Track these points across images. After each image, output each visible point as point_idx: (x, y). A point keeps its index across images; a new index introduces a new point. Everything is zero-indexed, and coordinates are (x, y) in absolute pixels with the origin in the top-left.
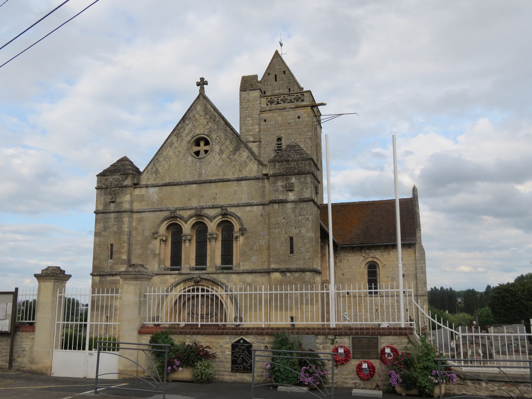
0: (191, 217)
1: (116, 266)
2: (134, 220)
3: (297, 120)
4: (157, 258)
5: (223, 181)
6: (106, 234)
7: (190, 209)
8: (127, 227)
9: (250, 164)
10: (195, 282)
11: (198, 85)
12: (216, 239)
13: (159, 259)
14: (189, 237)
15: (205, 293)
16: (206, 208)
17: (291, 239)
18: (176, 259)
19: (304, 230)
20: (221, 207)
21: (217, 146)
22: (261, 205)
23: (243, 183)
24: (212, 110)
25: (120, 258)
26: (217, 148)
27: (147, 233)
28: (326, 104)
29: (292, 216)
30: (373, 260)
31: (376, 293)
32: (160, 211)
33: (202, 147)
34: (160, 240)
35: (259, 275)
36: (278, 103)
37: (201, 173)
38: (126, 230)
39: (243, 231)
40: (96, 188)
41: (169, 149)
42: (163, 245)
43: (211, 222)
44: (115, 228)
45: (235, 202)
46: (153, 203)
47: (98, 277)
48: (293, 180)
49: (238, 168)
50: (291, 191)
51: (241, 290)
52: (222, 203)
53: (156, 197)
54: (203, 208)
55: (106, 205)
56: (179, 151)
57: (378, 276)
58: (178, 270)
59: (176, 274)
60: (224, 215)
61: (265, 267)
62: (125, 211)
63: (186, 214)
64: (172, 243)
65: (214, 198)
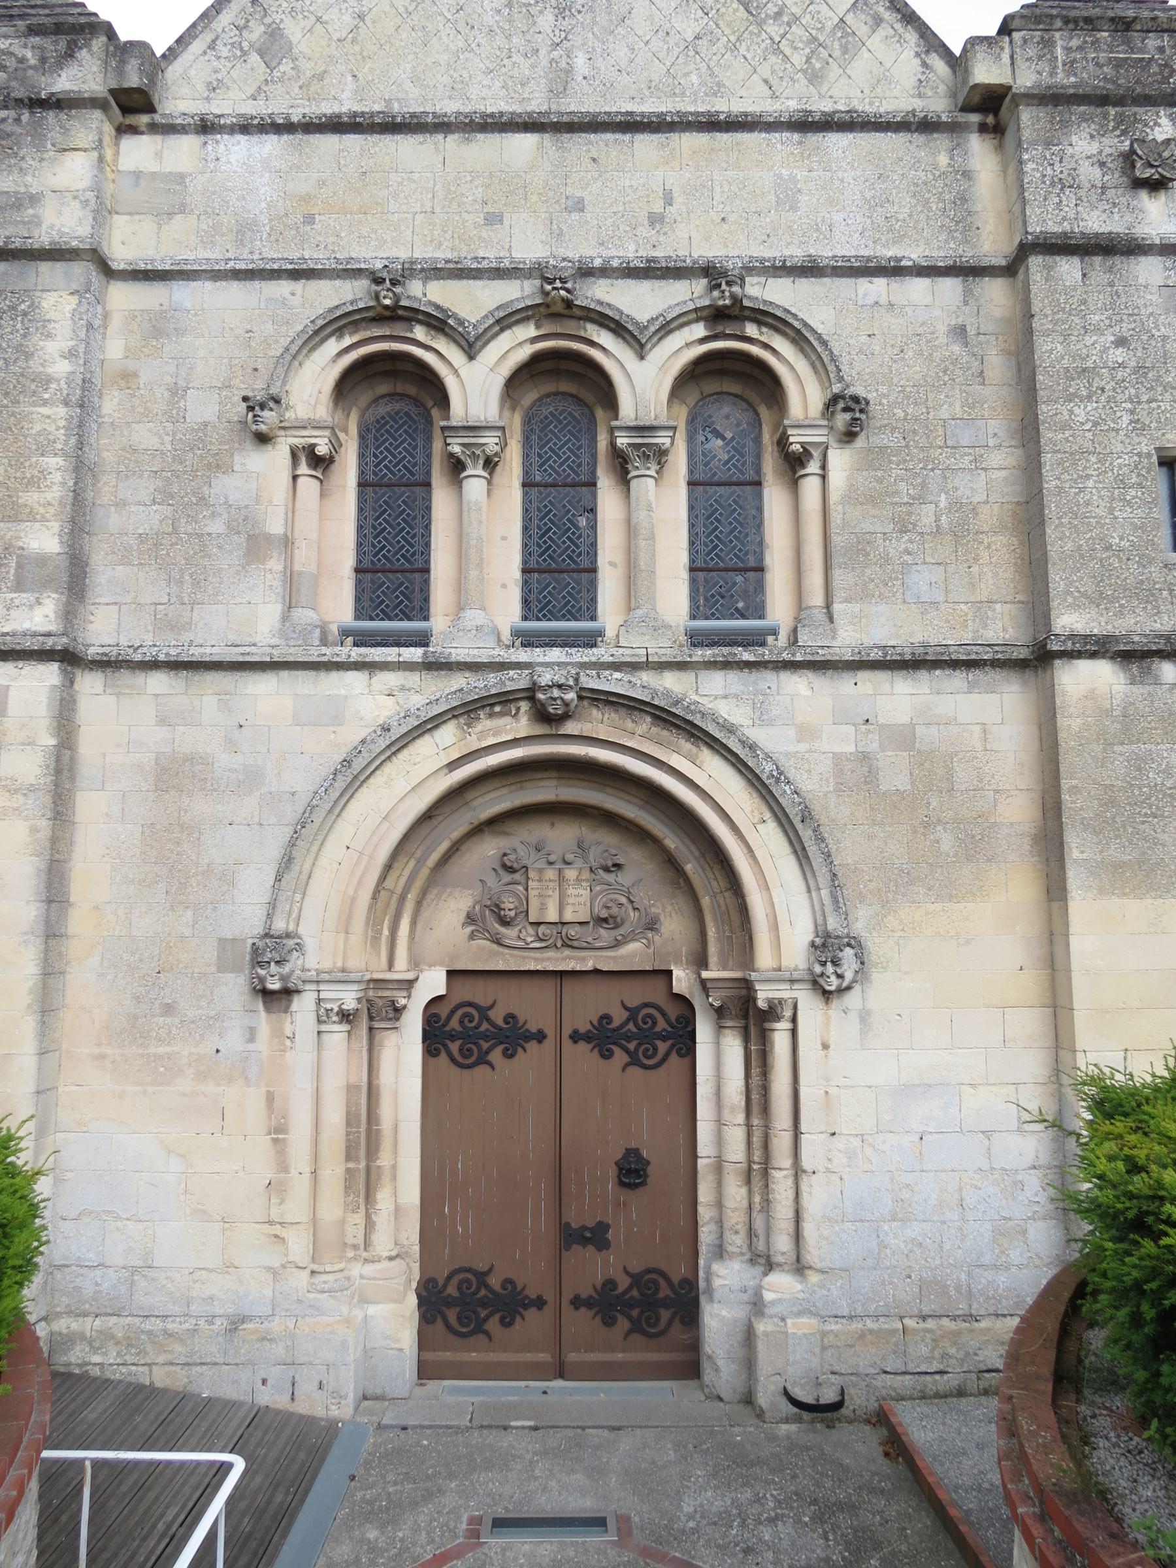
0: (506, 320)
4: (275, 564)
5: (712, 124)
7: (499, 273)
8: (71, 354)
13: (291, 579)
16: (605, 272)
18: (393, 578)
20: (711, 273)
23: (837, 142)
27: (209, 408)
32: (296, 274)
35: (959, 679)
37: (569, 71)
38: (61, 368)
39: (849, 412)
42: (308, 486)
45: (795, 253)
46: (244, 230)
49: (798, 59)
58: (422, 640)
59: (409, 666)
62: (57, 254)
63: (471, 302)
65: (655, 220)
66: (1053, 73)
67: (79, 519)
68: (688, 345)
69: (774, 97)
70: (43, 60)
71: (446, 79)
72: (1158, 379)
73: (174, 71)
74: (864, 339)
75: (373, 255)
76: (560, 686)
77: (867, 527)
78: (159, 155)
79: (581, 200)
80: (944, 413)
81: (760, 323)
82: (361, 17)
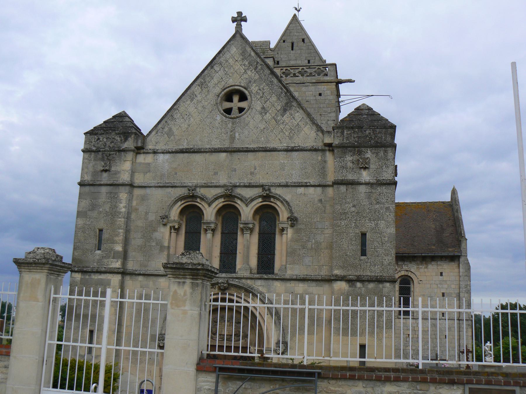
1: (106, 261)
2: (135, 197)
3: (319, 98)
4: (166, 253)
5: (265, 150)
6: (95, 214)
7: (216, 187)
8: (125, 207)
9: (306, 129)
10: (220, 289)
11: (233, 21)
12: (251, 230)
14: (213, 226)
15: (227, 304)
16: (239, 186)
17: (364, 235)
19: (382, 224)
20: (262, 186)
21: (259, 102)
22: (319, 186)
23: (295, 154)
24: (253, 54)
25: (112, 249)
26: (257, 105)
27: (152, 217)
28: (354, 81)
29: (366, 202)
30: (406, 273)
31: (407, 313)
32: (172, 187)
33: (236, 103)
34: (171, 227)
35: (314, 284)
36: (295, 75)
37: (234, 138)
38: (123, 210)
39: (293, 220)
40: (83, 151)
41: (189, 102)
42: (174, 235)
43: (247, 205)
44: (107, 207)
45: (283, 181)
46: (162, 175)
47: (80, 274)
48: (369, 154)
49: (287, 133)
50: (365, 168)
51: (286, 302)
52: (263, 181)
53: (166, 166)
54: (236, 186)
55: (95, 174)
56: (203, 107)
57: (412, 294)
60: (266, 198)
61: (324, 272)
62: (123, 185)
64: (186, 233)
66: (343, 140)
67: (126, 242)
68: (258, 203)
69: (281, 143)
70: (121, 140)
71: (207, 140)
72: (362, 215)
73: (149, 139)
74: (298, 202)
75: (189, 182)
76: (223, 283)
77: (296, 247)
78: (145, 159)
79: (235, 169)
80: (315, 220)
81: (274, 198)
82: (189, 125)
